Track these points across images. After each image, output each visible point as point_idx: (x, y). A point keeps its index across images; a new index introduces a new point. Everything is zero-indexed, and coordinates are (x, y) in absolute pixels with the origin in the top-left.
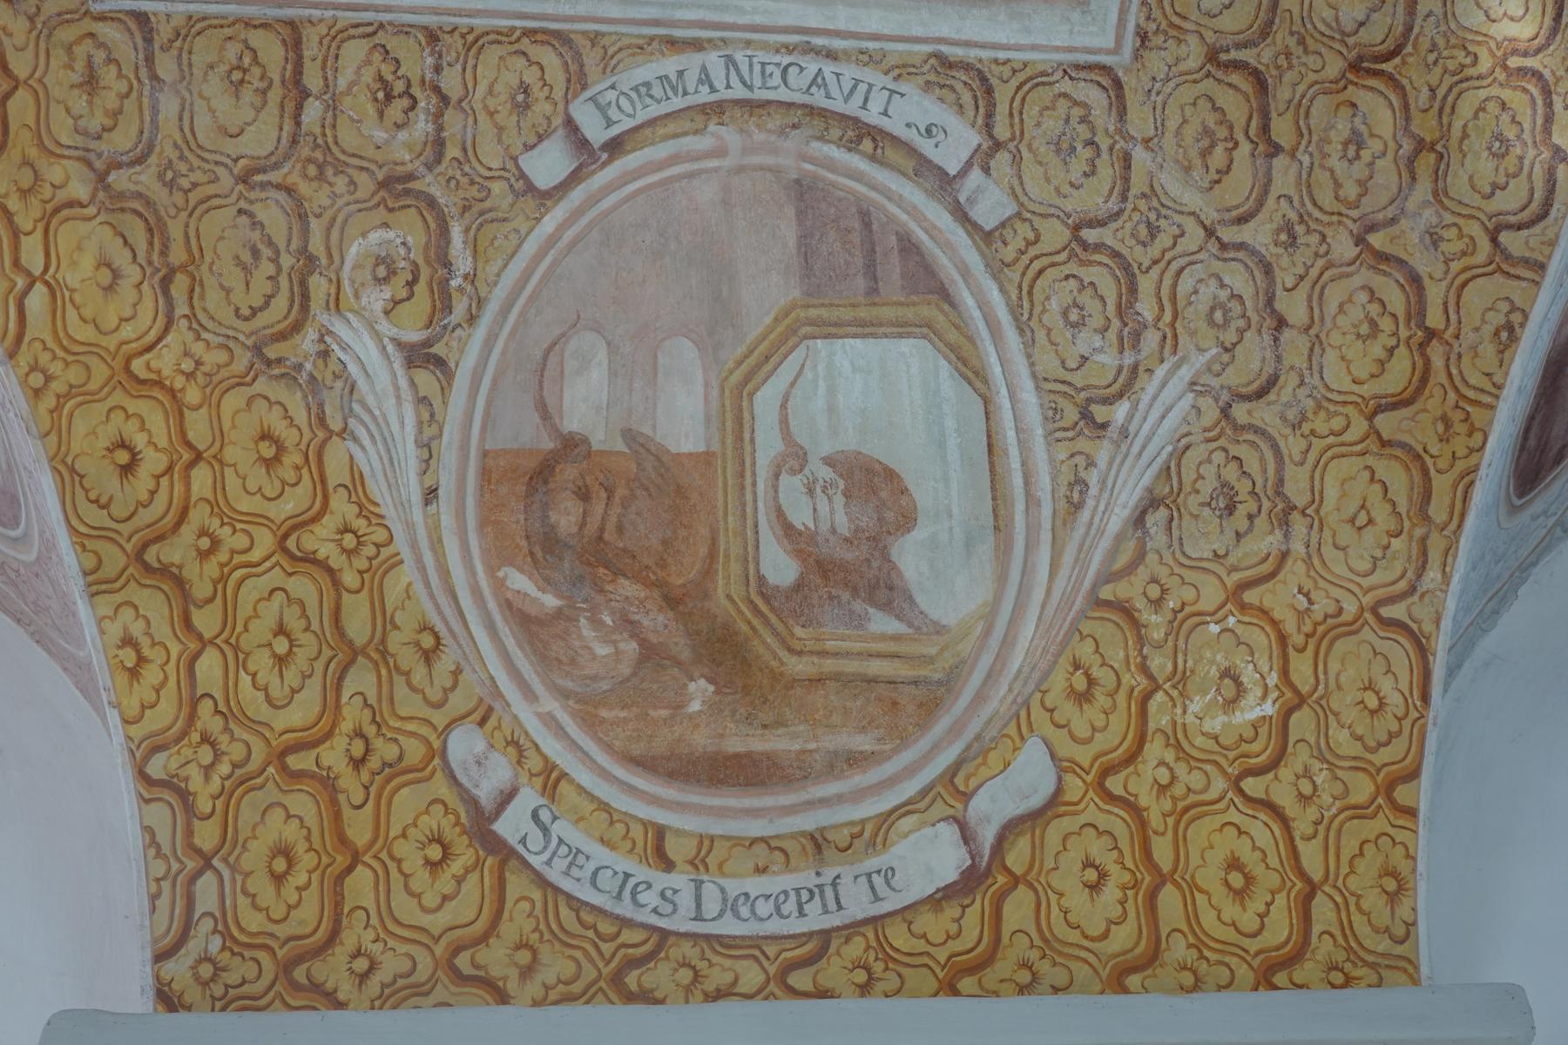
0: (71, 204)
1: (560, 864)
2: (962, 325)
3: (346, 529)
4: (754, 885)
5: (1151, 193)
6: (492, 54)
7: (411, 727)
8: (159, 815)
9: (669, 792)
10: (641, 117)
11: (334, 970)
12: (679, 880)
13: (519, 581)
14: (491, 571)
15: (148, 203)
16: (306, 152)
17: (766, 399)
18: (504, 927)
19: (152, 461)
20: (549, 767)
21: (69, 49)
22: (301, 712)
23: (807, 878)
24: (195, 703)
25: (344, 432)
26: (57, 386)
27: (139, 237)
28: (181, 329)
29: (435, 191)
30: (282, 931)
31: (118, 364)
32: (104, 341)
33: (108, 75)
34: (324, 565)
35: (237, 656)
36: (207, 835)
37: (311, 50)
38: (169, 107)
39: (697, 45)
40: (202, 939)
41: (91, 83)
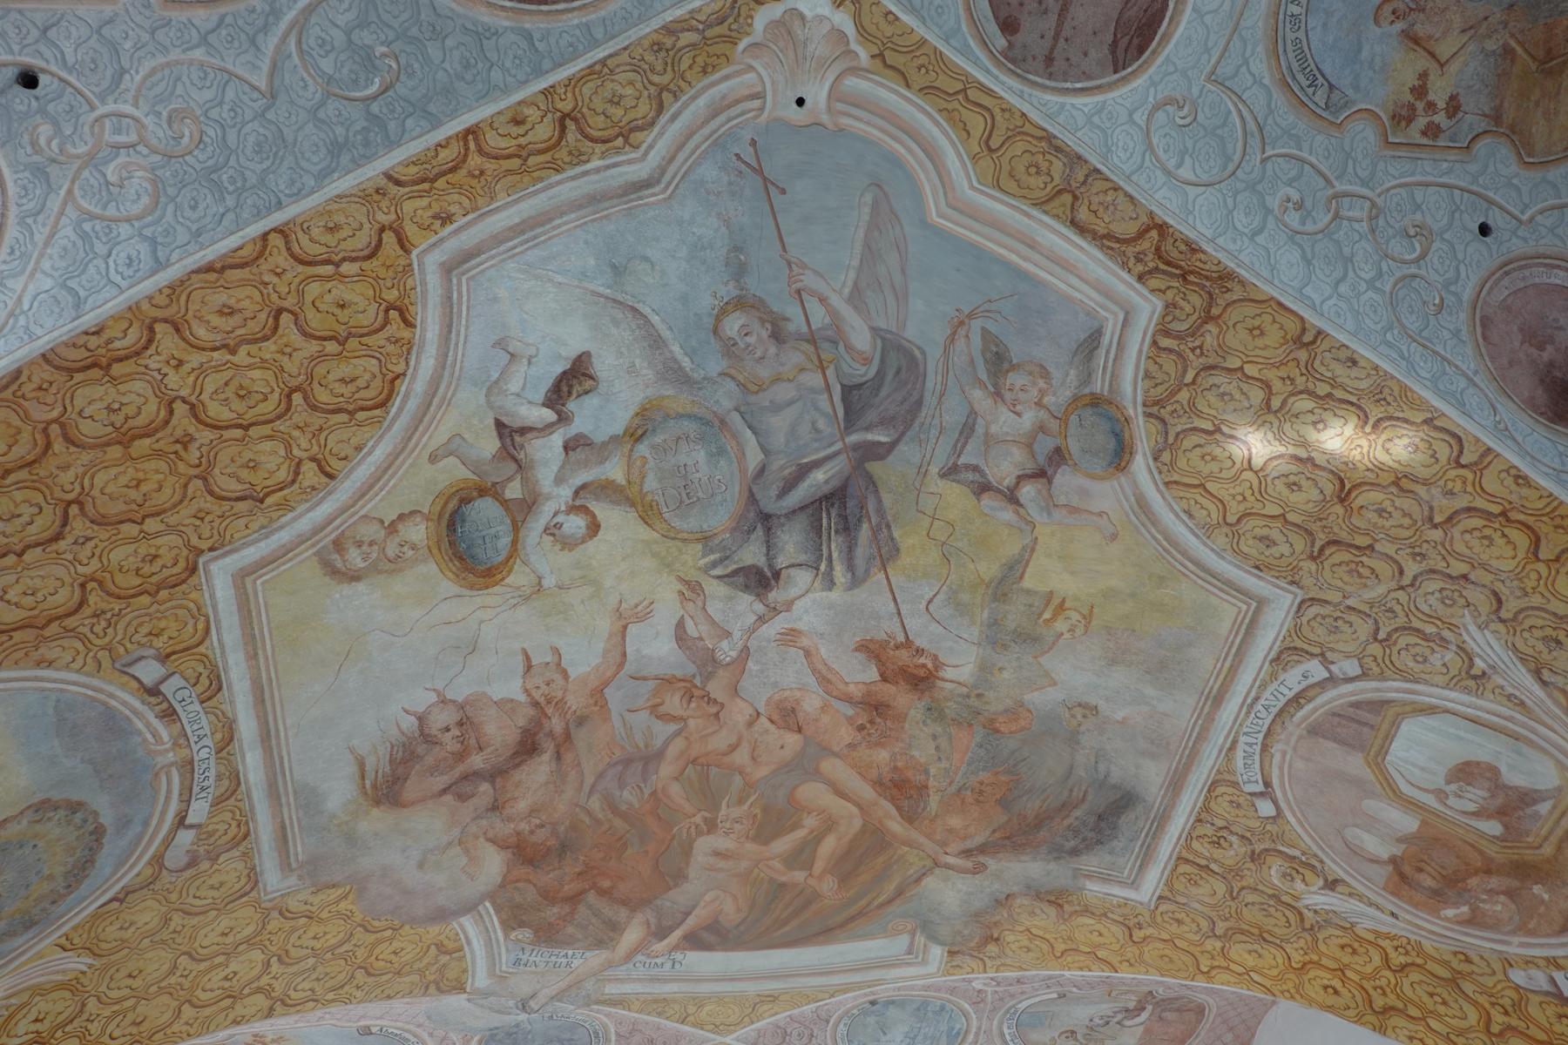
2: (1405, 703)
6: (1212, 804)
7: (1499, 987)
14: (1439, 918)
16: (1229, 877)
17: (1405, 788)
19: (1337, 984)
20: (1547, 959)
22: (1473, 1016)
27: (1244, 938)
29: (1262, 847)
33: (1178, 916)
39: (1235, 742)
41: (1179, 922)
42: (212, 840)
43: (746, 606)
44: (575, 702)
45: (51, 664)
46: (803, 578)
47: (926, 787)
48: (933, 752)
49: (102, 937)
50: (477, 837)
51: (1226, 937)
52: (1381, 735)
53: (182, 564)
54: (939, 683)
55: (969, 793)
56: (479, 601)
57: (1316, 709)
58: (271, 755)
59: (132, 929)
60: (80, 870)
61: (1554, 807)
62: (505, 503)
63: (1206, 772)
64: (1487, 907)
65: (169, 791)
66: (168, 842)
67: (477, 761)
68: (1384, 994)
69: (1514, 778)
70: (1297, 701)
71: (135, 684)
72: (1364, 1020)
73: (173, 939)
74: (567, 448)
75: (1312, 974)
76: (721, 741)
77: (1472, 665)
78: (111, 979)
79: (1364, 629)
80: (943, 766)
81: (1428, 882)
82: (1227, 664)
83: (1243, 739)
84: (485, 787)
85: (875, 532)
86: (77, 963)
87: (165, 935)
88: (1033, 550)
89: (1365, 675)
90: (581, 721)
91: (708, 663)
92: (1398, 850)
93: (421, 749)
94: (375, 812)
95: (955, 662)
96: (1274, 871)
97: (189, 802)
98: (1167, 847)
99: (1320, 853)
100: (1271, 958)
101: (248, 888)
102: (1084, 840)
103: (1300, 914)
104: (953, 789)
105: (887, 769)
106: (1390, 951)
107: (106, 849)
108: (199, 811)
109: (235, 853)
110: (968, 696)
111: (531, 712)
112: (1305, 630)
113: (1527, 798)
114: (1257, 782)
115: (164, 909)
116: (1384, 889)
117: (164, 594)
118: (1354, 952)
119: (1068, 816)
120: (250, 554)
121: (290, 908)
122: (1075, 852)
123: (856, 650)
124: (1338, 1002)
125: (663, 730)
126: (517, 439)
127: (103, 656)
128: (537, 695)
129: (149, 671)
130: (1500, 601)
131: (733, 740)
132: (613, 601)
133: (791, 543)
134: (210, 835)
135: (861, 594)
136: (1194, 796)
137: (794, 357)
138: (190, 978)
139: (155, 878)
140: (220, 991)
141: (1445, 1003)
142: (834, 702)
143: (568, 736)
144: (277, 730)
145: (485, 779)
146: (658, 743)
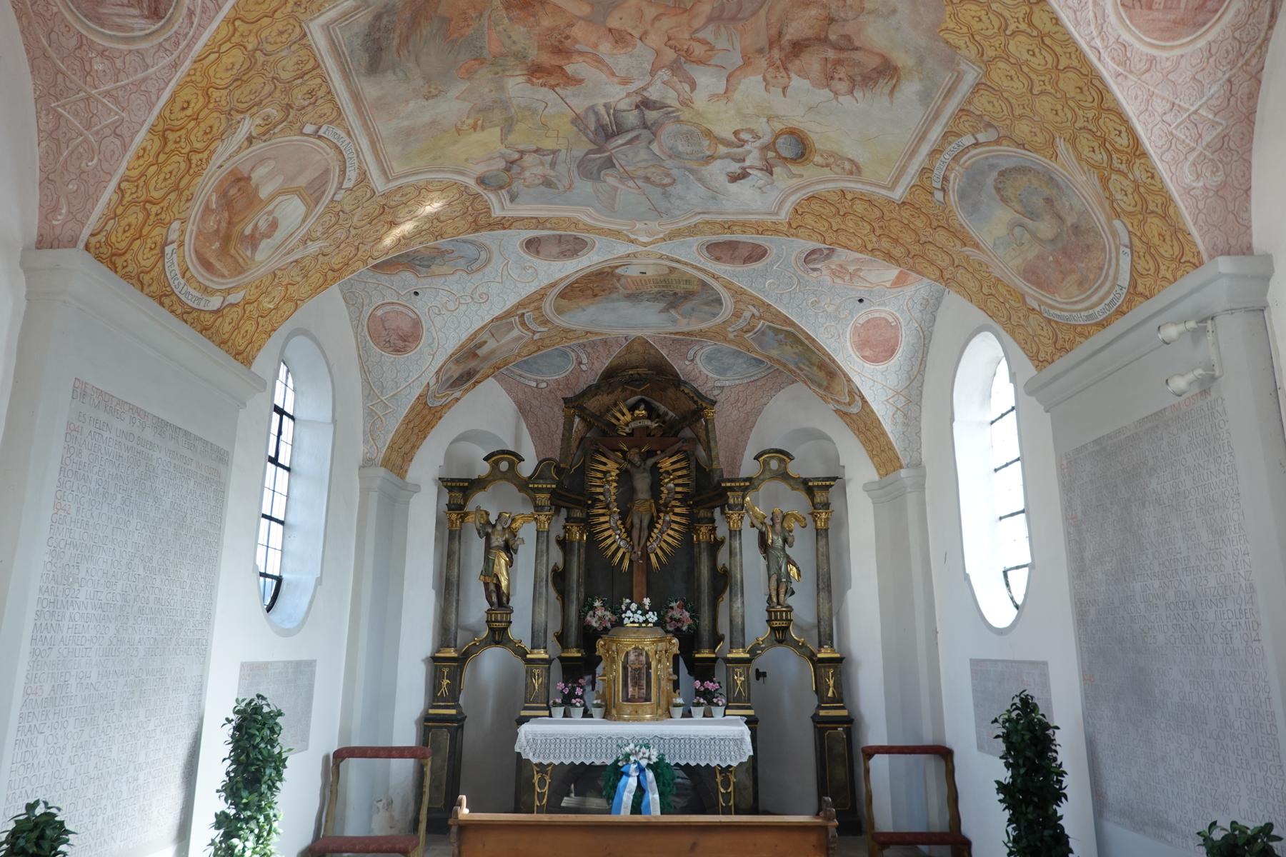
0: (245, 47)
1: (169, 264)
2: (312, 211)
3: (201, 160)
4: (192, 291)
5: (353, 215)
6: (331, 105)
7: (171, 214)
8: (115, 197)
9: (195, 262)
10: (330, 137)
11: (120, 262)
12: (183, 281)
13: (214, 198)
14: (213, 191)
15: (255, 63)
16: (287, 85)
17: (281, 198)
18: (152, 273)
19: (189, 112)
20: (183, 241)
21: (289, 23)
22: (156, 195)
23: (198, 294)
24: (143, 175)
25: (223, 140)
26: (193, 78)
27: (245, 67)
28: (225, 92)
29: (291, 114)
30: (117, 245)
31: (208, 86)
32: (212, 78)
33: (285, 36)
34: (191, 164)
35: (159, 172)
36: (119, 211)
37: (314, 73)
38: (283, 54)
39: (350, 136)
40: (101, 237)
41: (281, 33)
42: (975, 124)
43: (654, 93)
44: (762, 62)
45: (961, 225)
46: (622, 106)
47: (506, 9)
48: (511, 34)
49: (1044, 142)
50: (851, 6)
51: (251, 56)
52: (306, 197)
53: (906, 207)
54: (525, 72)
55: (474, 15)
56: (800, 125)
57: (334, 175)
58: (926, 129)
59: (1033, 130)
60: (1021, 170)
61: (247, 257)
62: (776, 151)
63: (349, 114)
64: (213, 218)
65: (969, 159)
66: (987, 144)
67: (831, 54)
68: (176, 142)
69: (264, 244)
70: (343, 171)
71: (946, 198)
72: (160, 120)
73: (1028, 105)
74: (744, 160)
75: (201, 98)
76: (666, 23)
77: (311, 240)
78: (1062, 122)
79: (347, 209)
80: (501, 27)
81: (232, 192)
82: (381, 155)
83: (348, 140)
84: (833, 37)
85: (587, 127)
86: (1061, 146)
87: (1028, 112)
88: (502, 139)
89: (332, 201)
90: (760, 51)
91: (675, 68)
92: (253, 183)
93: (858, 78)
94: (900, 65)
95: (521, 86)
96: (273, 112)
97: (968, 147)
98: (330, 64)
99: (270, 142)
100: (223, 78)
101: (983, 87)
102: (379, 30)
103: (242, 112)
104: (486, 13)
105: (540, 14)
106: (200, 156)
107: (1006, 166)
108: (968, 140)
109: (972, 109)
110: (503, 71)
111: (789, 66)
112: (365, 189)
113: (254, 248)
114: (325, 133)
115: (1017, 122)
116: (236, 167)
117: (917, 206)
118: (206, 133)
119: (400, 36)
120: (884, 192)
121: (976, 52)
122: (378, 17)
123: (583, 80)
124: (177, 108)
125: (707, 34)
126: (765, 168)
127: (947, 211)
128: (784, 74)
129: (939, 195)
130: (324, 255)
131: (657, 24)
132: (730, 104)
133: (632, 118)
134: (973, 127)
135: (588, 103)
136: (342, 99)
137: (641, 173)
138: (1043, 78)
139: (1005, 137)
140: (1043, 52)
141: (165, 179)
142: (591, 51)
143: (771, 45)
144: (916, 136)
145: (830, 40)
146: (711, 27)
